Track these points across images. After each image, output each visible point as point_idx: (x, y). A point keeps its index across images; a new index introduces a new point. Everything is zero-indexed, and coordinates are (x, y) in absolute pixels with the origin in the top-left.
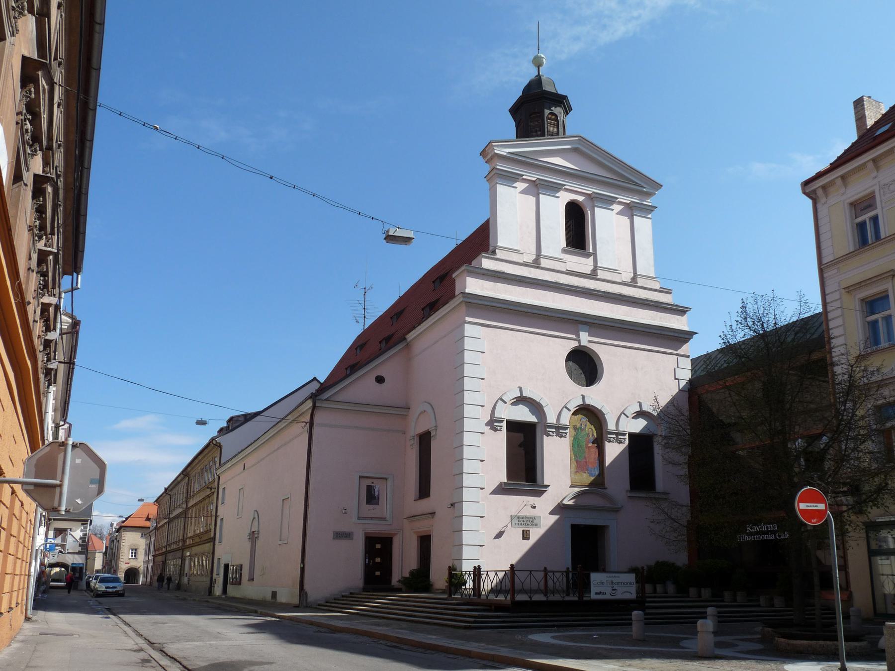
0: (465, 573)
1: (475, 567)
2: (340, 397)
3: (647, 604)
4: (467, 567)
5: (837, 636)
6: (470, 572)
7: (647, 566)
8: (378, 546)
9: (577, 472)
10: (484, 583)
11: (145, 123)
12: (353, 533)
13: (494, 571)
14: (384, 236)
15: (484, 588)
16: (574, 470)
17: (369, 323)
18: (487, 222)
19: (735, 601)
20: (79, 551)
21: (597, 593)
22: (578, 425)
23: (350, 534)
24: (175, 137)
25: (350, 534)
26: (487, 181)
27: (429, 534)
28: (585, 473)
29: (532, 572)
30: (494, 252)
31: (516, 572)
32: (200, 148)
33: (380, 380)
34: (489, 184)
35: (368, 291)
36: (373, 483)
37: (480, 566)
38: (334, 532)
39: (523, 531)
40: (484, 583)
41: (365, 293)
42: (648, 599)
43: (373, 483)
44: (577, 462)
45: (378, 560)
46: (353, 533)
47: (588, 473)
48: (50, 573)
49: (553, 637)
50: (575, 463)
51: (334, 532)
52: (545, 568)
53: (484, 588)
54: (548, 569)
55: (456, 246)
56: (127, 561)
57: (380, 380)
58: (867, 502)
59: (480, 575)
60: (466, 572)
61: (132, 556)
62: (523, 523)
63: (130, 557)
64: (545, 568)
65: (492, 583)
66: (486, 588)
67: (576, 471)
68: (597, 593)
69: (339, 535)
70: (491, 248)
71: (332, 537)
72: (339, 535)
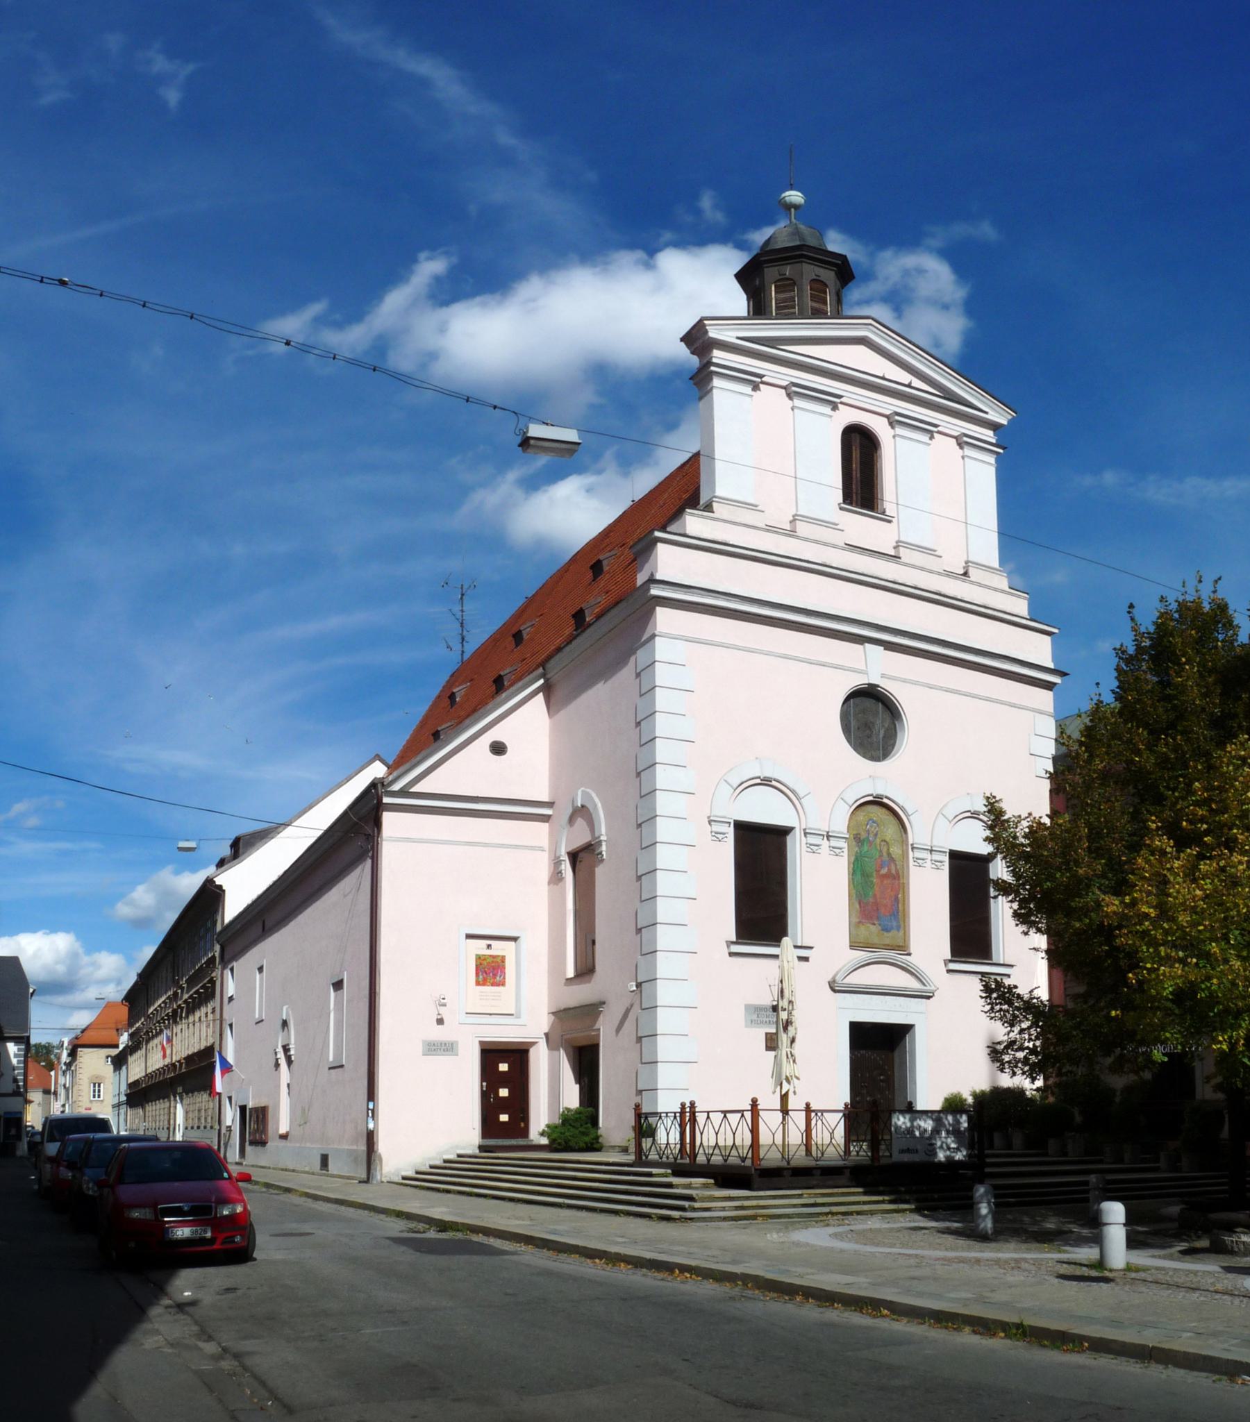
0: (665, 1115)
1: (683, 1105)
2: (416, 789)
3: (988, 1170)
4: (667, 1103)
5: (262, 1107)
6: (675, 1113)
7: (975, 1095)
8: (503, 1067)
9: (860, 922)
10: (702, 1134)
11: (42, 277)
12: (457, 1042)
13: (722, 1112)
14: (519, 440)
15: (701, 1143)
16: (855, 920)
17: (470, 648)
18: (696, 456)
19: (1009, 1146)
20: (14, 1091)
21: (902, 1151)
22: (864, 835)
23: (452, 1044)
24: (99, 292)
25: (452, 1044)
26: (695, 384)
27: (595, 1042)
28: (874, 924)
29: (728, 1115)
30: (709, 508)
31: (761, 1113)
32: (147, 305)
33: (498, 749)
34: (699, 390)
35: (469, 592)
36: (489, 946)
37: (694, 1103)
38: (424, 1042)
39: (766, 1034)
40: (702, 1134)
41: (463, 595)
42: (988, 1160)
43: (489, 946)
44: (860, 904)
45: (504, 1092)
46: (457, 1042)
47: (880, 925)
48: (1030, 1007)
49: (835, 1236)
50: (858, 906)
51: (424, 1042)
52: (808, 1105)
53: (701, 1143)
54: (813, 1107)
55: (632, 503)
56: (88, 1105)
57: (498, 749)
58: (1063, 1007)
59: (693, 1120)
60: (667, 1113)
61: (94, 1096)
62: (765, 1019)
63: (92, 1098)
64: (808, 1105)
65: (734, 1134)
66: (705, 1144)
67: (858, 920)
68: (902, 1151)
69: (433, 1048)
70: (703, 500)
71: (421, 1050)
72: (433, 1048)
